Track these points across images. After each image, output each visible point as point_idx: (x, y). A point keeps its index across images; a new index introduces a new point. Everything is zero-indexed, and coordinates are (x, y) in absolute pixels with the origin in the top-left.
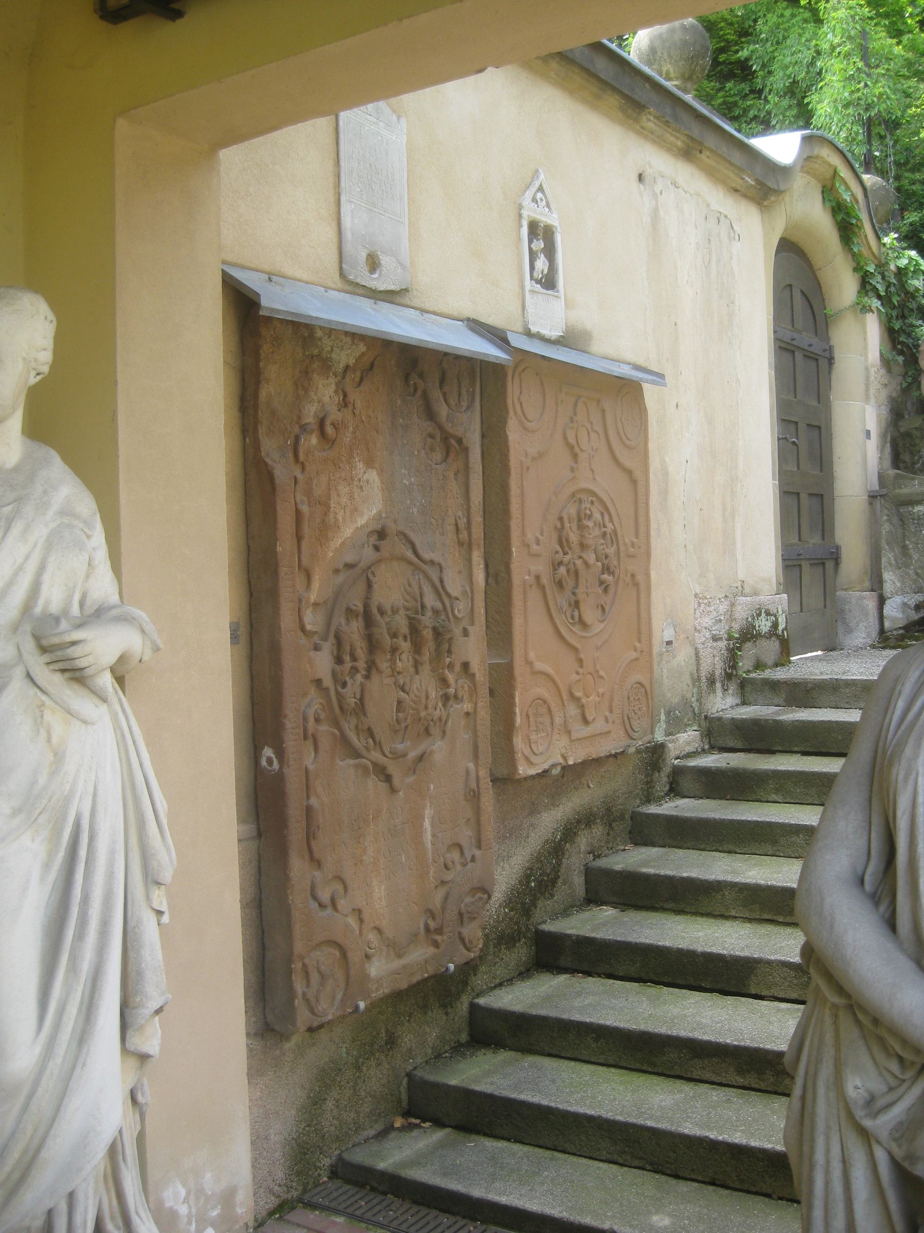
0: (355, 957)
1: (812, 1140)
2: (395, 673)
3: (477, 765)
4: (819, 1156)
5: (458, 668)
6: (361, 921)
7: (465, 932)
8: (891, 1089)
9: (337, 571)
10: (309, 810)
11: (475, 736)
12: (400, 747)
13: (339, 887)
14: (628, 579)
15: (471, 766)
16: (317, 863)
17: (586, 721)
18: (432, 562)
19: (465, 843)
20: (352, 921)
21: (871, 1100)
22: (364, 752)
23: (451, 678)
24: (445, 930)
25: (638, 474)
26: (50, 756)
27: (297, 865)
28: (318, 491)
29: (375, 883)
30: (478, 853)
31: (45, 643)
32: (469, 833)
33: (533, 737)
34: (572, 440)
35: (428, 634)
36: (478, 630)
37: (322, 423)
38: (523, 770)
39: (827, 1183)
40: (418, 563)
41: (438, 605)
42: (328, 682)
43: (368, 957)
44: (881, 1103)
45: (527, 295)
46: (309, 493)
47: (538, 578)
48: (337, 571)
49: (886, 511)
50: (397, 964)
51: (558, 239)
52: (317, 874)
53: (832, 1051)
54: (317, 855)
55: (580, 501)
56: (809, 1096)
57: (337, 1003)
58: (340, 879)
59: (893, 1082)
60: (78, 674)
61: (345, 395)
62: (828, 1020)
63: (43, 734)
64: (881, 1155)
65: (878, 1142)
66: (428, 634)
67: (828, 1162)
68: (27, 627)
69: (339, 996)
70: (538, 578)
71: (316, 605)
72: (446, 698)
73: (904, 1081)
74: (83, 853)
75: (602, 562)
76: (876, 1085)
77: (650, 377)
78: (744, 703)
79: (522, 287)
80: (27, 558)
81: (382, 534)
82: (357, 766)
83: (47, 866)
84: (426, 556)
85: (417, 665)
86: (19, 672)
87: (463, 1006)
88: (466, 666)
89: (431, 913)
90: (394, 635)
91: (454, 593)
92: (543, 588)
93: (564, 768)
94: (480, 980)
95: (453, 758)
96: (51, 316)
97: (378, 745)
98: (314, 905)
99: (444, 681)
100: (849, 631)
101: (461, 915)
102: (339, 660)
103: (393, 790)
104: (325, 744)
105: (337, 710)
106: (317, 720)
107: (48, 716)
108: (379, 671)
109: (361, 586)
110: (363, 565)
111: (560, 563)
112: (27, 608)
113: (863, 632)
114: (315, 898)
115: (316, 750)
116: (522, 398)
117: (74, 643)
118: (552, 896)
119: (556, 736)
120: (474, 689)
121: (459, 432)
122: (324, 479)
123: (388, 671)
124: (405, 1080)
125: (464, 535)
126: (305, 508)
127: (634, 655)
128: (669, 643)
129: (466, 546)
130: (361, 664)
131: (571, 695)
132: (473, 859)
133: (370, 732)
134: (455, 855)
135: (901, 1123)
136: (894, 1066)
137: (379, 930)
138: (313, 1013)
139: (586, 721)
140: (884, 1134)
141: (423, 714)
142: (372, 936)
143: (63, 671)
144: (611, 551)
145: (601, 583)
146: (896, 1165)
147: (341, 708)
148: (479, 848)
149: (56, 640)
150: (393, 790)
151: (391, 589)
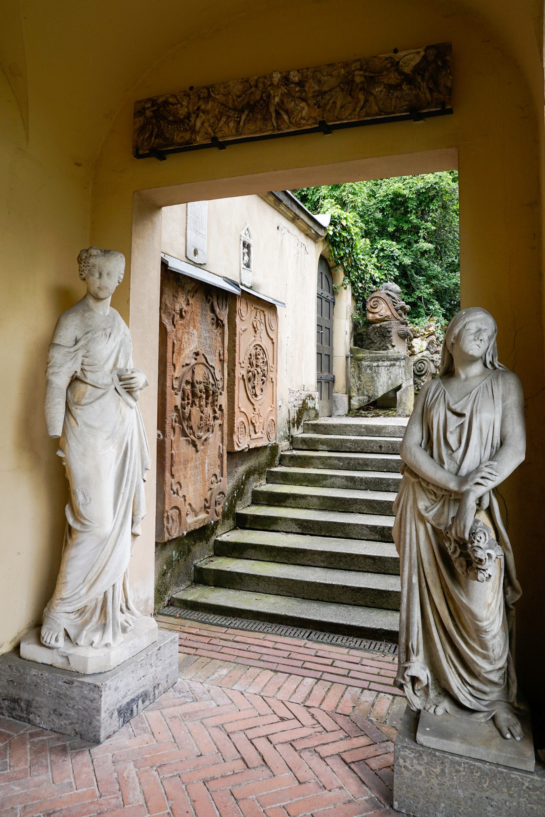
0: (183, 514)
1: (405, 526)
2: (200, 406)
3: (223, 445)
4: (408, 530)
5: (218, 407)
6: (185, 500)
7: (217, 508)
8: (432, 505)
9: (183, 366)
10: (172, 455)
11: (222, 434)
12: (201, 434)
13: (179, 486)
14: (270, 380)
15: (221, 445)
16: (172, 476)
17: (256, 433)
18: (212, 366)
19: (218, 474)
20: (182, 499)
21: (427, 508)
22: (189, 435)
23: (217, 410)
24: (211, 507)
25: (274, 341)
26: (121, 419)
27: (168, 475)
28: (179, 336)
29: (190, 486)
30: (222, 478)
31: (123, 377)
32: (219, 471)
33: (239, 436)
34: (255, 326)
35: (211, 392)
36: (225, 393)
37: (181, 310)
38: (237, 449)
39: (411, 539)
40: (207, 365)
41: (213, 383)
42: (179, 407)
43: (187, 515)
44: (429, 509)
45: (242, 269)
46: (176, 336)
47: (243, 376)
48: (183, 366)
49: (353, 363)
50: (196, 519)
51: (252, 249)
52: (173, 480)
53: (412, 497)
54: (173, 473)
55: (256, 349)
56: (404, 512)
57: (177, 531)
58: (179, 483)
59: (433, 502)
60: (131, 390)
61: (188, 301)
62: (411, 488)
63: (119, 409)
64: (428, 525)
65: (429, 522)
66: (211, 392)
67: (411, 532)
68: (116, 372)
69: (178, 529)
70: (243, 376)
71: (176, 378)
72: (215, 418)
73: (436, 501)
74: (129, 454)
75: (260, 372)
76: (428, 504)
77: (279, 304)
78: (304, 433)
79: (240, 266)
80: (115, 347)
81: (197, 354)
82: (187, 440)
83: (117, 458)
84: (211, 364)
85: (207, 403)
86: (113, 387)
87: (214, 538)
88: (221, 406)
89: (206, 500)
90: (201, 392)
91: (218, 379)
92: (244, 380)
93: (249, 449)
94: (219, 531)
95: (215, 441)
96: (491, 318)
97: (194, 433)
98: (172, 492)
99: (215, 412)
100: (337, 409)
101: (216, 502)
102: (183, 399)
103: (197, 451)
104: (177, 430)
105: (182, 418)
106: (175, 421)
107: (121, 403)
108: (196, 405)
109: (191, 372)
110: (191, 365)
111: (250, 371)
112: (115, 365)
113: (343, 408)
114: (172, 489)
115: (174, 433)
116: (241, 306)
117: (132, 378)
118: (241, 500)
119: (246, 437)
120: (222, 416)
121: (222, 318)
122: (181, 331)
123: (198, 405)
124: (193, 568)
125: (222, 357)
126: (175, 341)
127: (271, 409)
128: (280, 406)
129: (222, 361)
130: (190, 401)
131: (251, 421)
132: (220, 481)
133: (191, 428)
134: (214, 478)
135: (435, 515)
136: (433, 498)
137: (190, 504)
138: (170, 535)
139: (256, 433)
140: (430, 518)
141: (208, 423)
142: (188, 507)
143: (125, 388)
144: (266, 368)
145: (262, 380)
146: (433, 527)
147: (183, 417)
148: (222, 476)
149: (127, 377)
150: (197, 451)
151: (200, 374)
